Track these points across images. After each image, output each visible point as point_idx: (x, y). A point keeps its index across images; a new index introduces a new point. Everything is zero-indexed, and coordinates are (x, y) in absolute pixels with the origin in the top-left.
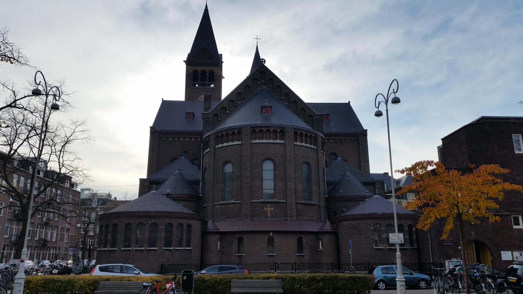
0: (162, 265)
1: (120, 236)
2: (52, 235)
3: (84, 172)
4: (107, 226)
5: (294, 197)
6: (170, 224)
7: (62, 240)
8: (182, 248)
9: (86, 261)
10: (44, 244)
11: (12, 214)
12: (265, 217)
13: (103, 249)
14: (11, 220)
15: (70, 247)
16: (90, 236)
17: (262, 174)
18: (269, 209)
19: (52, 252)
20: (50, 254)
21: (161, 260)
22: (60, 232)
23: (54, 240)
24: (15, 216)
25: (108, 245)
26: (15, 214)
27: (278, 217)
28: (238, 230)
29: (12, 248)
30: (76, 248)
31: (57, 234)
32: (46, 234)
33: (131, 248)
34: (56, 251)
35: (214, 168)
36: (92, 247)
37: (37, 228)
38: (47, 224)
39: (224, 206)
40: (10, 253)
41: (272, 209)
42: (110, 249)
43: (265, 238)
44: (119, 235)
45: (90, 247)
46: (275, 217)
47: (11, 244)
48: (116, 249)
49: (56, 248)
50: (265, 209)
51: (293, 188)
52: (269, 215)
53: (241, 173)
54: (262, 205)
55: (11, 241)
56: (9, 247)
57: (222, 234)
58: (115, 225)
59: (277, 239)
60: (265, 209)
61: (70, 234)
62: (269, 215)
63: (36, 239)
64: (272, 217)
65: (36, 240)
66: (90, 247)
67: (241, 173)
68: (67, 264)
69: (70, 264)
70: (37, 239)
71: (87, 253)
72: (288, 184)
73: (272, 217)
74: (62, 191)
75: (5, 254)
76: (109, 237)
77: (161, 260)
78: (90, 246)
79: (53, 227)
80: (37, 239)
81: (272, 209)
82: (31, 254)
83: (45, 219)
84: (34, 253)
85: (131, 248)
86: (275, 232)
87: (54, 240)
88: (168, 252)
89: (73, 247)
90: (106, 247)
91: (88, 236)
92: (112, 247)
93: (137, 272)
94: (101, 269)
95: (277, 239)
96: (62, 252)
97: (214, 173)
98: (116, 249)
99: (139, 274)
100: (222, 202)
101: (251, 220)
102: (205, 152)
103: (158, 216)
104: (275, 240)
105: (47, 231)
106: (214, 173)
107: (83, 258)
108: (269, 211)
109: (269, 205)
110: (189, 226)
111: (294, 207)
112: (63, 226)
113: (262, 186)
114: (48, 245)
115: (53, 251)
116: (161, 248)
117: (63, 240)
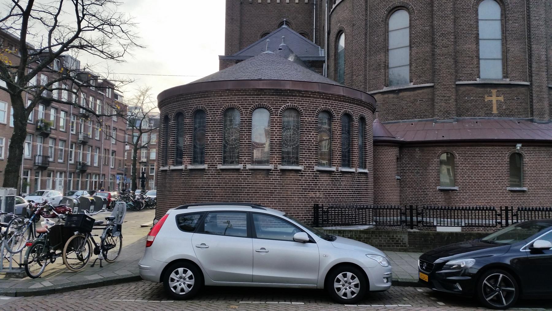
0: (316, 207)
1: (213, 138)
2: (92, 158)
3: (124, 27)
4: (179, 115)
5: (544, 74)
6: (327, 112)
7: (106, 164)
8: (353, 170)
9: (138, 192)
10: (82, 170)
11: (34, 126)
12: (487, 114)
13: (172, 168)
14: (33, 134)
15: (118, 174)
16: (143, 162)
17: (477, 27)
18: (494, 99)
19: (94, 180)
20: (91, 183)
21: (312, 194)
22: (103, 155)
23: (96, 165)
24: (37, 129)
25: (186, 159)
26: (37, 126)
27: (513, 115)
28: (440, 138)
29: (38, 173)
30: (126, 175)
31: (100, 158)
32: (84, 156)
33: (240, 166)
34: (99, 179)
35: (366, 24)
36: (145, 175)
37: (72, 148)
38: (84, 143)
39: (391, 95)
40: (36, 180)
41: (501, 98)
42: (190, 167)
43: (505, 154)
44: (209, 135)
45: (143, 175)
46: (508, 115)
47: (35, 168)
48: (205, 166)
49: (99, 175)
50: (487, 99)
51: (543, 58)
52: (495, 111)
53: (432, 27)
54: (479, 90)
55: (35, 163)
56: (34, 172)
57: (402, 146)
58: (199, 113)
59: (530, 159)
60: (487, 99)
61: (116, 157)
62: (495, 111)
63: (70, 162)
64: (500, 115)
65: (70, 164)
66: (143, 175)
67: (432, 27)
68: (110, 196)
69: (114, 196)
70: (72, 162)
71: (139, 182)
72: (534, 47)
73: (500, 115)
74: (102, 101)
75: (28, 180)
76: (186, 141)
77: (312, 194)
78: (143, 173)
79: (94, 147)
80: (72, 162)
81: (501, 98)
82: (65, 182)
83: (81, 137)
84: (70, 181)
85: (240, 166)
86: (527, 143)
87: (96, 165)
88: (325, 177)
89: (122, 174)
90: (181, 163)
91: (140, 163)
92: (194, 161)
93: (302, 236)
94: (184, 224)
95: (530, 159)
96: (109, 180)
97: (366, 34)
98: (205, 166)
99: (312, 241)
100: (385, 89)
101: (457, 121)
102: (334, 6)
103: (299, 92)
104: (526, 160)
105: (85, 152)
106: (366, 34)
107: (135, 188)
108: (494, 102)
109: (494, 91)
110: (362, 119)
111: (546, 96)
112: (107, 147)
113: (478, 51)
114: (88, 171)
115: (96, 178)
116: (310, 167)
117: (108, 165)
